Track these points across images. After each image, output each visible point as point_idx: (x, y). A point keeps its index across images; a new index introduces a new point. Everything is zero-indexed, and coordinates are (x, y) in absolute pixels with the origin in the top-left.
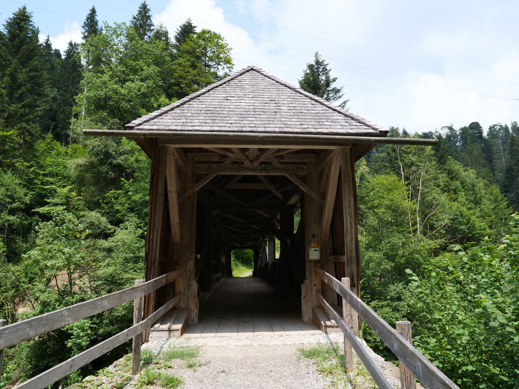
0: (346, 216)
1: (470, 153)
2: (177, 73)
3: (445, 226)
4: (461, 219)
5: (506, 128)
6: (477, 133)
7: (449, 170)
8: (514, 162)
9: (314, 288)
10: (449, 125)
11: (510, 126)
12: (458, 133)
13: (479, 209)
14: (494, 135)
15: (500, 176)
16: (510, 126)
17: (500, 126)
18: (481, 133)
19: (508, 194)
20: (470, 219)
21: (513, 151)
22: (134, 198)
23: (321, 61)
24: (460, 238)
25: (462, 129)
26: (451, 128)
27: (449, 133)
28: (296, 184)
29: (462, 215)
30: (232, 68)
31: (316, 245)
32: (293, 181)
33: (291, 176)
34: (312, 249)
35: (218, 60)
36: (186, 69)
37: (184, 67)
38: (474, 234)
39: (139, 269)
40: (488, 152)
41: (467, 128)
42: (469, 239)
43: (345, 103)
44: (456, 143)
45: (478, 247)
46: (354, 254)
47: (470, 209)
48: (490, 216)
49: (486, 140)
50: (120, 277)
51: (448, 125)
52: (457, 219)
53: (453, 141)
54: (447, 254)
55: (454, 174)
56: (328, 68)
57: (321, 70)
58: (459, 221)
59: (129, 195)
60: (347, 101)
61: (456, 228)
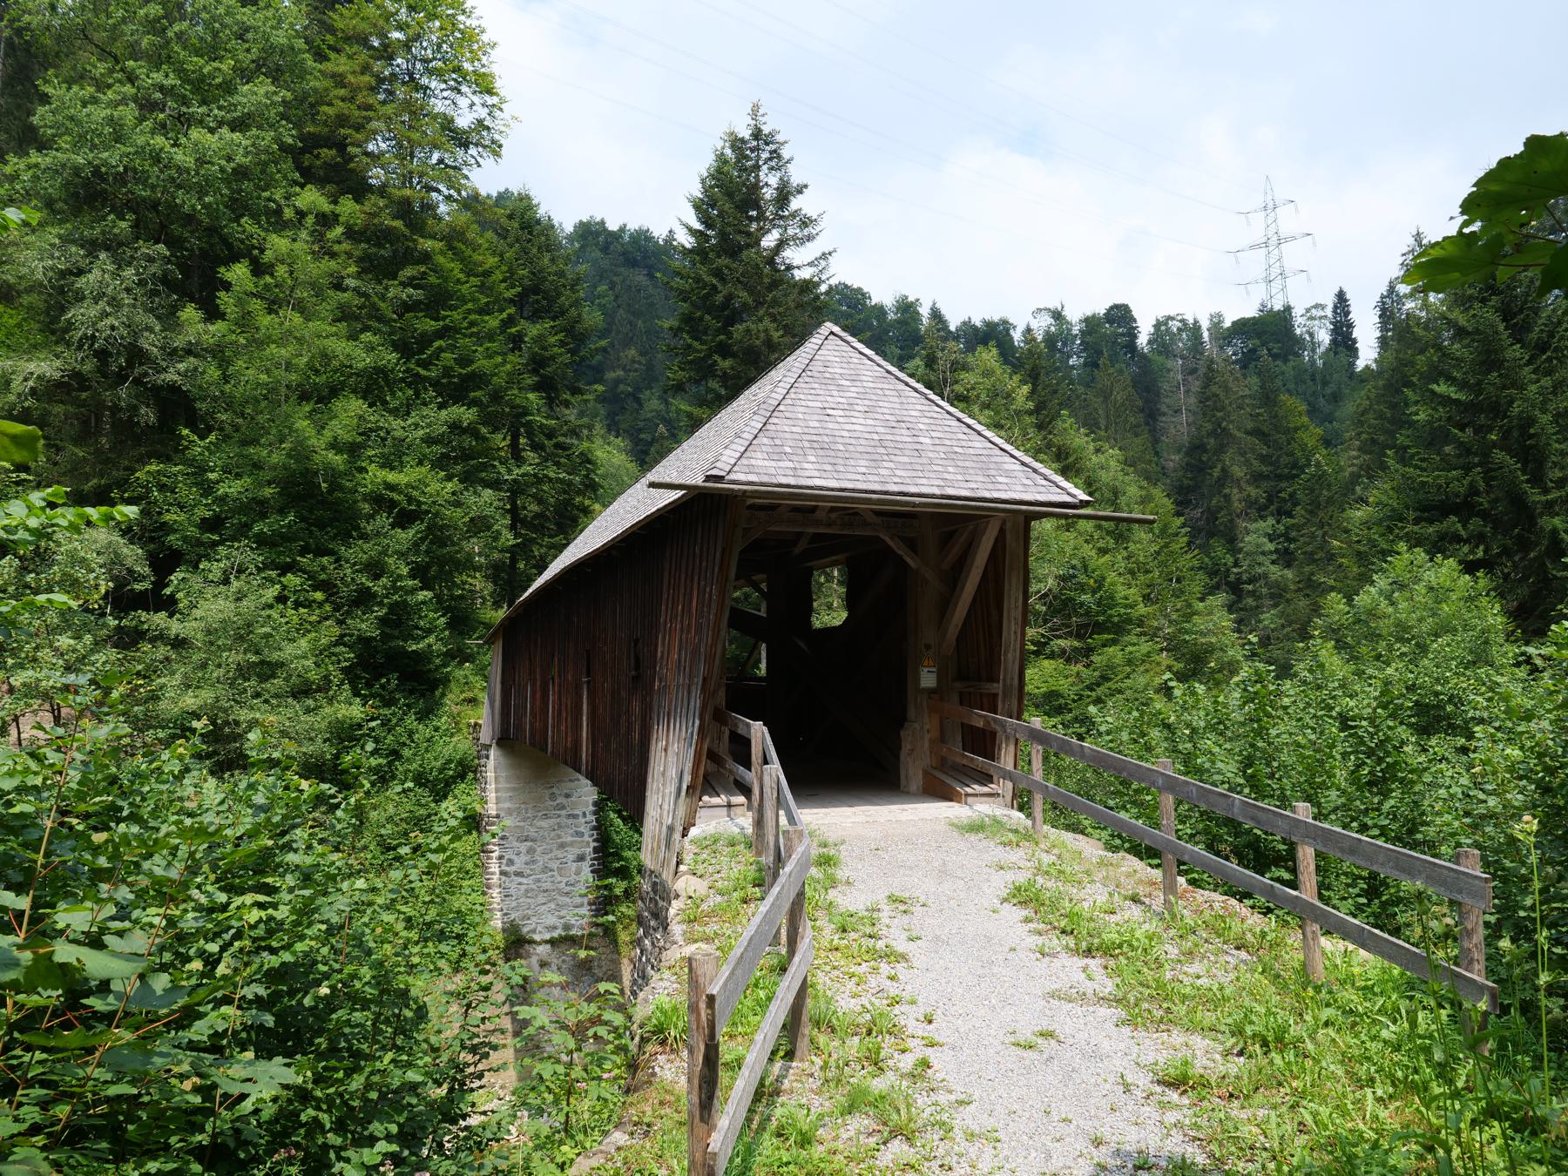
0: (1010, 621)
1: (1106, 395)
2: (330, 104)
3: (1045, 595)
4: (1082, 578)
5: (1196, 328)
6: (1123, 335)
7: (1059, 448)
8: (1209, 426)
9: (927, 737)
10: (1054, 304)
11: (1205, 324)
12: (1076, 330)
13: (1125, 554)
14: (1164, 344)
15: (1174, 460)
16: (1205, 324)
17: (1180, 321)
18: (1132, 334)
19: (1186, 511)
20: (1104, 579)
21: (1208, 399)
22: (222, 490)
23: (766, 130)
24: (1080, 626)
25: (1087, 320)
26: (1057, 315)
27: (1053, 329)
28: (900, 552)
29: (1085, 567)
30: (501, 110)
31: (931, 663)
32: (895, 548)
33: (892, 539)
34: (926, 670)
35: (457, 76)
36: (360, 99)
37: (355, 90)
38: (1111, 616)
39: (276, 696)
40: (1147, 390)
41: (1100, 318)
42: (1099, 628)
43: (824, 256)
44: (1070, 357)
45: (1118, 648)
46: (1016, 681)
47: (1103, 551)
48: (1147, 572)
49: (1143, 356)
50: (231, 718)
51: (1052, 307)
52: (1074, 576)
53: (1060, 351)
54: (1046, 663)
55: (1071, 459)
56: (785, 153)
57: (765, 155)
58: (1079, 583)
59: (208, 480)
60: (830, 254)
61: (1071, 600)
